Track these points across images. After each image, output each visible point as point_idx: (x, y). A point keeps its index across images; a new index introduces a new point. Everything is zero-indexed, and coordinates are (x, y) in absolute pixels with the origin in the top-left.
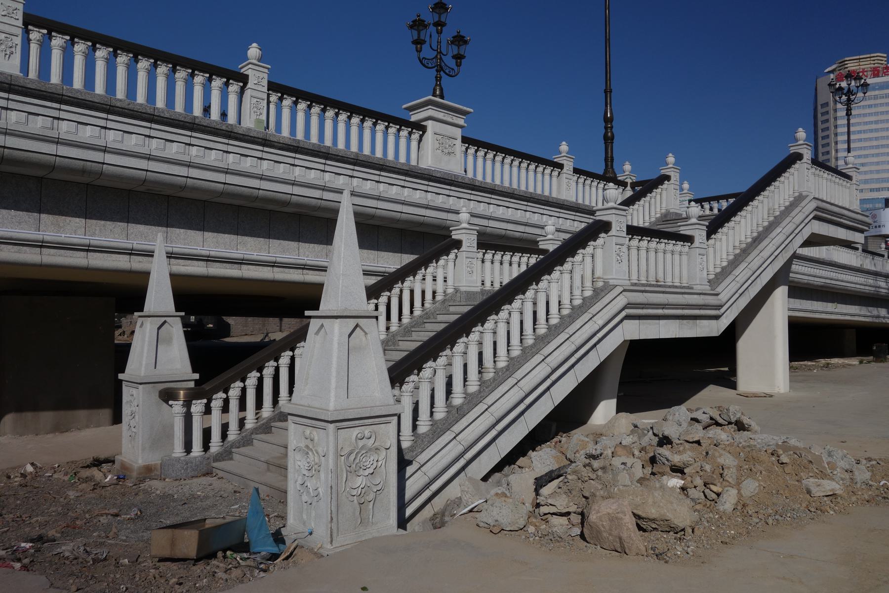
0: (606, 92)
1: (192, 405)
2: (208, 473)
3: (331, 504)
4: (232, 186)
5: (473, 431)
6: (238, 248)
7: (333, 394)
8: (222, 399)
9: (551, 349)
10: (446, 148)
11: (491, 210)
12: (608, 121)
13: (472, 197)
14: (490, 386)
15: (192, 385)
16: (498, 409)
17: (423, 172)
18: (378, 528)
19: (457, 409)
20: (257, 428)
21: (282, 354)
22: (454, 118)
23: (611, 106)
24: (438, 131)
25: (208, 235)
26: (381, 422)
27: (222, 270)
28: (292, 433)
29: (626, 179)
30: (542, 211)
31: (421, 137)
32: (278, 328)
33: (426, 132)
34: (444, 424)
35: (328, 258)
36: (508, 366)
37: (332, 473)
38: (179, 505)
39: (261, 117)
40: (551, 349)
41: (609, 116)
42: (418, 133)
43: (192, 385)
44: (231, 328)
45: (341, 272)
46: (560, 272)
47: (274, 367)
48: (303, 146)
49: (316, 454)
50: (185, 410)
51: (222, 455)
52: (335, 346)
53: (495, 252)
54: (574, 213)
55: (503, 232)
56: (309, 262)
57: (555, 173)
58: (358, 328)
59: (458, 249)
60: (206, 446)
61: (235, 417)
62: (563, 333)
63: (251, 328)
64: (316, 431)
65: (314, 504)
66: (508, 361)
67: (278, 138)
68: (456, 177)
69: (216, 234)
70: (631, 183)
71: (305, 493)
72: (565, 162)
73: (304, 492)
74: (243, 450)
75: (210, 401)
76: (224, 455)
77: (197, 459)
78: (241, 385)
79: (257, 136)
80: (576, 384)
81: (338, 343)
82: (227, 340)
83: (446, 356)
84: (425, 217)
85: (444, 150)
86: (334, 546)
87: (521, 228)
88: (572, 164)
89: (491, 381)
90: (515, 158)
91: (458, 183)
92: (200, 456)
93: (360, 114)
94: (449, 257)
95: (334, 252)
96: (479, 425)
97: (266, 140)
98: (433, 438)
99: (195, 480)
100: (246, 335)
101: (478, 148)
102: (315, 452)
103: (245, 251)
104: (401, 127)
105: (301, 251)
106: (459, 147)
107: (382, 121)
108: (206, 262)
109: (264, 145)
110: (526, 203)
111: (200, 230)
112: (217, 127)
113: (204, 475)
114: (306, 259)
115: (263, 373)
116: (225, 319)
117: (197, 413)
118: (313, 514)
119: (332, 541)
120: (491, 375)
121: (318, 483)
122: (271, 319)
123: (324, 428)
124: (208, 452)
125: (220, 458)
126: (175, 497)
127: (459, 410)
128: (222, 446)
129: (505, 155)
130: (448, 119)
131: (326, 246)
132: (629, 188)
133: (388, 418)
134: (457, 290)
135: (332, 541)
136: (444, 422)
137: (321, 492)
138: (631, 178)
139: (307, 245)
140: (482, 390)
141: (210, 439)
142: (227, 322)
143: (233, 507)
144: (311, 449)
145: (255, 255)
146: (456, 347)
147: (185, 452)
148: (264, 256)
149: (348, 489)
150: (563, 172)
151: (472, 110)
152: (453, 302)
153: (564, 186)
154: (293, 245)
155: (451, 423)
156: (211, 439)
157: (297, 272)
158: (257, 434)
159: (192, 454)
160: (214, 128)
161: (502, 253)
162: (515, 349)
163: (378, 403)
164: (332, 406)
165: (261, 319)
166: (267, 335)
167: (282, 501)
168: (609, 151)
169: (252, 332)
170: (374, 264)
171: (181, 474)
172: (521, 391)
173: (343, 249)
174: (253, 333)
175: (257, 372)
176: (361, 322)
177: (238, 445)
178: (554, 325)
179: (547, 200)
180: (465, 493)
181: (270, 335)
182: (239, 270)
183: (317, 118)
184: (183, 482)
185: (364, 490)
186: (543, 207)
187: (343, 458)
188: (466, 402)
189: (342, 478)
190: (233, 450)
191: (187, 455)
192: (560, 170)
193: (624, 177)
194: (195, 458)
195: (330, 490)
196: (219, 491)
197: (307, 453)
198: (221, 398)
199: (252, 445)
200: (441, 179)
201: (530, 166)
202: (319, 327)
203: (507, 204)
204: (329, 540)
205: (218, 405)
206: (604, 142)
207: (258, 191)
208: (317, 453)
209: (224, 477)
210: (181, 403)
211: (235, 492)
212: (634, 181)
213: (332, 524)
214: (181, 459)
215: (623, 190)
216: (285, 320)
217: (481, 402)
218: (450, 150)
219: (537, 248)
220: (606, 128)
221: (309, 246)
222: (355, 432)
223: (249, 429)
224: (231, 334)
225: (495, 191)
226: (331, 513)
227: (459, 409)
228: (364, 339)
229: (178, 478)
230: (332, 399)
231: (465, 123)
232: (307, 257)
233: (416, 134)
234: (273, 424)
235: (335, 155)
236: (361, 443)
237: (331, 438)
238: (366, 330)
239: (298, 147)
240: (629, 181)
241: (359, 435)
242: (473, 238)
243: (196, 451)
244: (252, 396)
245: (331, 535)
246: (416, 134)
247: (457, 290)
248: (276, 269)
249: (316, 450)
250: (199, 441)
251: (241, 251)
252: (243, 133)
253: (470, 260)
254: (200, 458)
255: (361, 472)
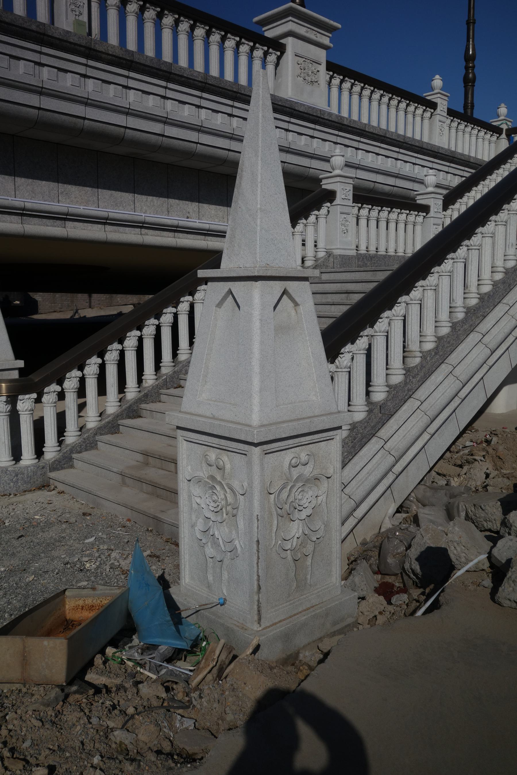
0: (468, 23)
1: (19, 401)
2: (45, 486)
3: (258, 566)
4: (49, 113)
5: (404, 436)
6: (60, 199)
7: (256, 400)
8: (56, 393)
9: (489, 325)
10: (308, 75)
11: (359, 157)
12: (469, 59)
13: (339, 140)
14: (418, 374)
15: (15, 375)
16: (433, 405)
17: (284, 104)
18: (319, 592)
19: (380, 406)
20: (101, 427)
21: (128, 334)
22: (318, 35)
23: (473, 41)
24: (299, 52)
25: (20, 181)
26: (322, 439)
27: (42, 227)
28: (185, 456)
29: (501, 124)
30: (414, 160)
31: (279, 58)
32: (87, 304)
33: (285, 52)
34: (365, 427)
35: (170, 214)
36: (437, 348)
37: (258, 520)
38: (14, 538)
39: (81, 18)
40: (489, 325)
41: (471, 53)
42: (275, 54)
43: (15, 375)
44: (39, 305)
45: (259, 206)
46: (495, 223)
47: (118, 351)
48: (138, 61)
49: (228, 490)
50: (9, 407)
51: (60, 462)
52: (256, 324)
53: (372, 207)
54: (448, 164)
55: (372, 185)
56: (148, 219)
57: (428, 115)
58: (285, 297)
59: (331, 201)
60: (39, 451)
61: (73, 415)
62: (500, 305)
63: (60, 305)
64: (228, 456)
65: (226, 562)
66: (436, 342)
67: (106, 47)
68: (322, 112)
69: (30, 180)
70: (507, 130)
71: (209, 544)
72: (438, 101)
73: (208, 542)
74: (85, 455)
75: (40, 396)
76: (63, 462)
77: (29, 469)
78: (79, 374)
79: (78, 43)
80: (510, 370)
81: (261, 320)
82: (36, 317)
83: (367, 336)
84: (286, 164)
85: (307, 78)
86: (263, 626)
87: (391, 181)
88: (446, 103)
89: (419, 368)
90: (385, 93)
91: (324, 121)
92: (33, 465)
93: (205, 24)
94: (320, 212)
95: (244, 173)
96: (411, 428)
97: (90, 49)
98: (354, 447)
99: (29, 496)
100: (55, 312)
101: (344, 78)
102: (226, 488)
103: (69, 204)
104: (255, 44)
105: (137, 204)
106: (323, 75)
107: (233, 34)
108: (20, 217)
109: (88, 57)
110: (397, 149)
111: (10, 175)
112: (25, 26)
113: (39, 489)
114: (143, 215)
115: (105, 359)
116: (32, 296)
117: (26, 411)
118: (225, 576)
119: (260, 620)
120: (418, 360)
121: (234, 532)
122: (80, 295)
123: (244, 452)
124: (42, 459)
125: (58, 466)
126: (7, 524)
127: (382, 408)
128: (59, 451)
129: (374, 89)
130: (311, 35)
131: (166, 199)
132: (504, 135)
133: (331, 433)
134: (329, 254)
135: (260, 620)
136: (366, 424)
137: (238, 547)
138: (507, 124)
139: (144, 198)
140: (408, 381)
141: (44, 442)
142: (34, 299)
143: (87, 541)
144: (220, 482)
145: (81, 209)
146: (378, 323)
147: (13, 460)
148: (91, 210)
149: (280, 542)
150: (435, 113)
151: (339, 26)
152: (326, 268)
153: (437, 131)
154: (127, 196)
155: (375, 426)
156: (45, 443)
157: (134, 232)
158: (101, 434)
159: (21, 462)
160: (21, 27)
161: (380, 208)
162: (443, 325)
163: (317, 412)
164: (255, 419)
165: (69, 295)
166: (77, 312)
167: (150, 529)
168: (470, 96)
169: (61, 309)
170: (224, 223)
171: (10, 488)
172: (458, 381)
173: (259, 168)
174: (61, 310)
175: (98, 357)
176: (291, 286)
177: (79, 449)
178: (485, 294)
179: (420, 146)
180: (456, 544)
181: (79, 311)
182: (62, 227)
183: (152, 24)
184: (14, 499)
185: (300, 539)
186: (416, 155)
187: (272, 496)
188: (390, 397)
189: (271, 526)
190: (74, 456)
191: (16, 464)
192: (432, 111)
193: (499, 123)
194: (27, 467)
195: (255, 546)
196: (62, 513)
197: (213, 488)
198: (55, 392)
199: (97, 448)
200: (305, 115)
201: (400, 104)
202: (223, 295)
203: (377, 150)
204: (256, 618)
205: (51, 400)
206: (463, 85)
207: (83, 120)
208: (231, 489)
209: (65, 492)
210: (4, 399)
211: (84, 514)
212: (510, 127)
213: (260, 595)
214: (9, 469)
215: (498, 137)
216: (95, 296)
217: (410, 397)
218: (313, 78)
219: (415, 203)
220: (467, 68)
221: (147, 198)
222: (287, 457)
223: (91, 429)
224: (39, 311)
225: (365, 133)
226: (258, 580)
227: (382, 406)
228: (293, 313)
229: (7, 492)
230: (256, 408)
231: (330, 42)
232: (144, 213)
233: (273, 55)
234: (120, 422)
235: (178, 75)
236: (295, 472)
237: (256, 468)
238: (297, 299)
239: (132, 61)
240: (504, 127)
241: (294, 461)
242: (348, 189)
243: (27, 458)
244: (93, 388)
245: (259, 611)
246: (273, 55)
247: (329, 254)
248: (108, 228)
249: (228, 485)
250: (30, 446)
251: (63, 203)
252: (60, 37)
253: (345, 216)
254: (32, 467)
255: (296, 515)
